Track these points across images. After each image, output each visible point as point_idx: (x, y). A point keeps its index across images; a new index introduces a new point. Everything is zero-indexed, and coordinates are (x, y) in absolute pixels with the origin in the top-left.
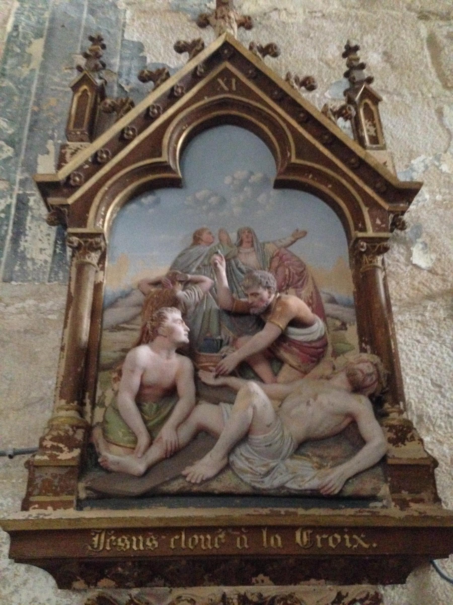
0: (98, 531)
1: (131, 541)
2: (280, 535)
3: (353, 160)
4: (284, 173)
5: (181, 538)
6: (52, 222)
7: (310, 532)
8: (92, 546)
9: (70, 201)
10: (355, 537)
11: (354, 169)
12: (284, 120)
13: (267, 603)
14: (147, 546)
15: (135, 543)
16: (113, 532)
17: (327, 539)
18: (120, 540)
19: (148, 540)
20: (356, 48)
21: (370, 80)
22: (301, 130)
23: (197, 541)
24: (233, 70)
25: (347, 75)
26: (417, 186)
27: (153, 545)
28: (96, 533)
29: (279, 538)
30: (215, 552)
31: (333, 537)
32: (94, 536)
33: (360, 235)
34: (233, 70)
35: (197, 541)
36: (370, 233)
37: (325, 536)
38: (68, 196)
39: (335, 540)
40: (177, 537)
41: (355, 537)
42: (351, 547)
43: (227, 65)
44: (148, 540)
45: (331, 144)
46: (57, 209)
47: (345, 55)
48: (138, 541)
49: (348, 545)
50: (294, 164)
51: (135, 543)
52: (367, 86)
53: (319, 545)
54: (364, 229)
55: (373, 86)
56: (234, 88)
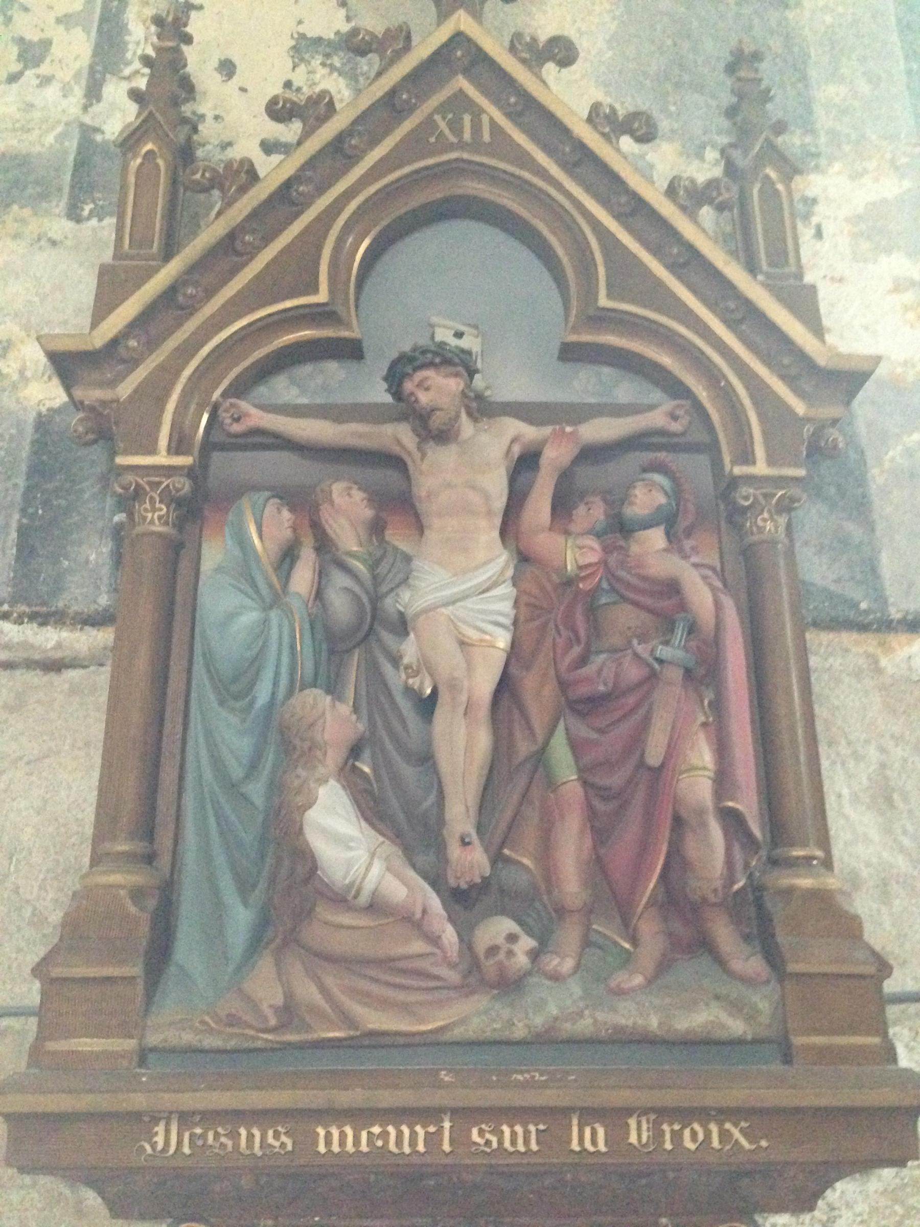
2: (606, 1127)
3: (732, 305)
4: (575, 329)
7: (653, 1117)
8: (154, 1145)
9: (125, 390)
10: (728, 1126)
14: (270, 1146)
15: (257, 1139)
16: (197, 1118)
19: (270, 1133)
20: (757, 56)
22: (625, 237)
23: (701, 1137)
24: (472, 92)
25: (731, 112)
26: (866, 367)
27: (283, 1145)
28: (155, 1120)
29: (601, 1132)
30: (416, 1160)
31: (692, 1129)
34: (472, 92)
35: (701, 1137)
36: (761, 468)
37: (677, 1127)
38: (112, 384)
39: (694, 1134)
40: (432, 1129)
41: (728, 1126)
43: (462, 83)
45: (684, 265)
46: (92, 409)
47: (731, 69)
50: (604, 309)
51: (257, 1139)
52: (772, 137)
53: (668, 1146)
54: (747, 457)
56: (486, 137)
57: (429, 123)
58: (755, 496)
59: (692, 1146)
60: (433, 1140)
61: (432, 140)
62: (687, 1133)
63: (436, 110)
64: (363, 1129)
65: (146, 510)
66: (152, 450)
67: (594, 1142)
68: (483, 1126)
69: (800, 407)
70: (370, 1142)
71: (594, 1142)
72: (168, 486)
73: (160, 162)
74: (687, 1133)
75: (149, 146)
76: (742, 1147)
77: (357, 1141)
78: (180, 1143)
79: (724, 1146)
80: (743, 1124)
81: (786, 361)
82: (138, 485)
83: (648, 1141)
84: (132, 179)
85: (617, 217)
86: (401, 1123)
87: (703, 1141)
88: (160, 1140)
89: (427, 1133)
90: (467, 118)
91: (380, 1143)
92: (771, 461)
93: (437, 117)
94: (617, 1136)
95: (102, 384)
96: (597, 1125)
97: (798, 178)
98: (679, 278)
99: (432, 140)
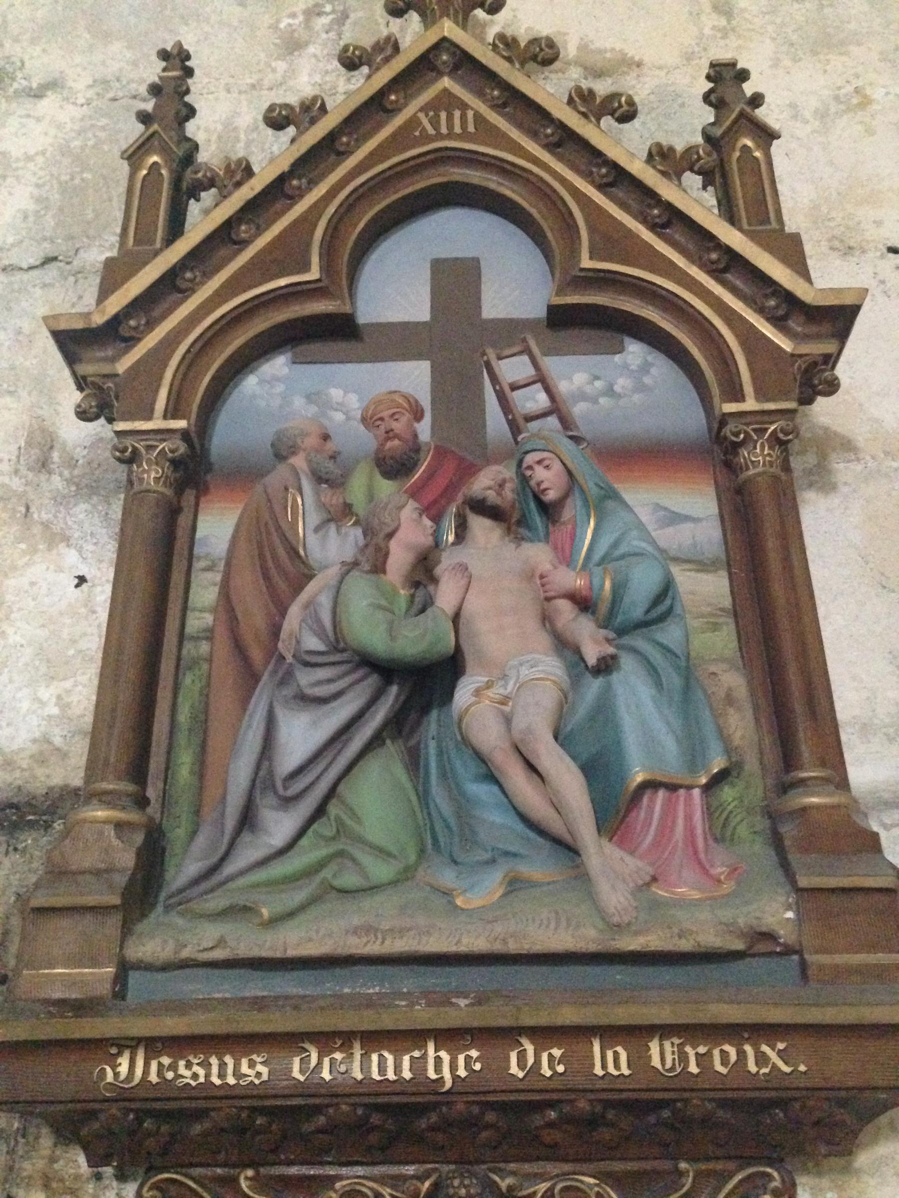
0: (129, 1043)
1: (206, 1065)
5: (424, 1056)
6: (84, 412)
9: (123, 366)
10: (765, 1048)
11: (716, 273)
12: (563, 181)
13: (540, 1195)
15: (215, 1070)
17: (709, 1054)
18: (182, 1063)
19: (244, 1062)
21: (757, 100)
23: (733, 1057)
24: (458, 90)
32: (120, 1054)
33: (730, 407)
34: (458, 90)
35: (531, 1061)
36: (750, 404)
37: (702, 1050)
38: (114, 360)
39: (724, 1055)
40: (417, 1054)
41: (765, 1048)
42: (758, 1072)
43: (446, 82)
44: (244, 1062)
48: (222, 1066)
49: (752, 1067)
51: (215, 1070)
54: (739, 397)
55: (761, 113)
56: (471, 128)
57: (413, 122)
58: (746, 432)
59: (723, 1070)
60: (418, 1065)
61: (417, 134)
62: (716, 1053)
63: (421, 109)
64: (545, 1050)
65: (144, 471)
66: (149, 417)
67: (617, 1066)
68: (254, 1057)
69: (785, 344)
70: (160, 1073)
71: (617, 1066)
72: (164, 448)
73: (164, 172)
74: (716, 1053)
75: (155, 158)
76: (779, 1070)
77: (398, 1068)
78: (146, 1071)
79: (760, 1069)
80: (781, 1046)
81: (772, 303)
82: (134, 447)
83: (674, 1064)
84: (138, 185)
85: (601, 188)
86: (225, 1054)
87: (736, 1063)
88: (124, 1069)
89: (697, 1054)
90: (457, 114)
91: (343, 1068)
92: (761, 394)
93: (421, 115)
94: (639, 1060)
95: (106, 360)
96: (386, 1054)
97: (775, 142)
98: (660, 236)
99: (417, 134)
